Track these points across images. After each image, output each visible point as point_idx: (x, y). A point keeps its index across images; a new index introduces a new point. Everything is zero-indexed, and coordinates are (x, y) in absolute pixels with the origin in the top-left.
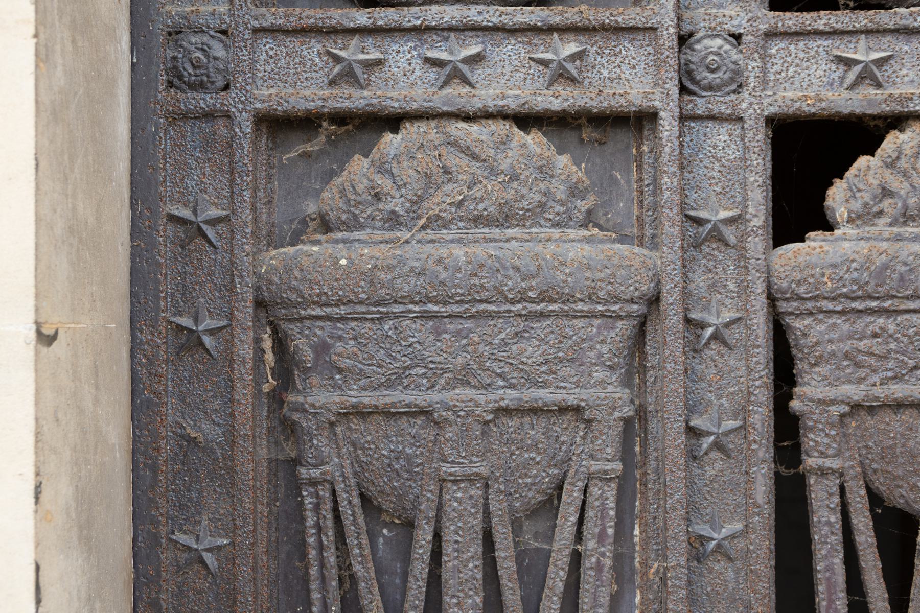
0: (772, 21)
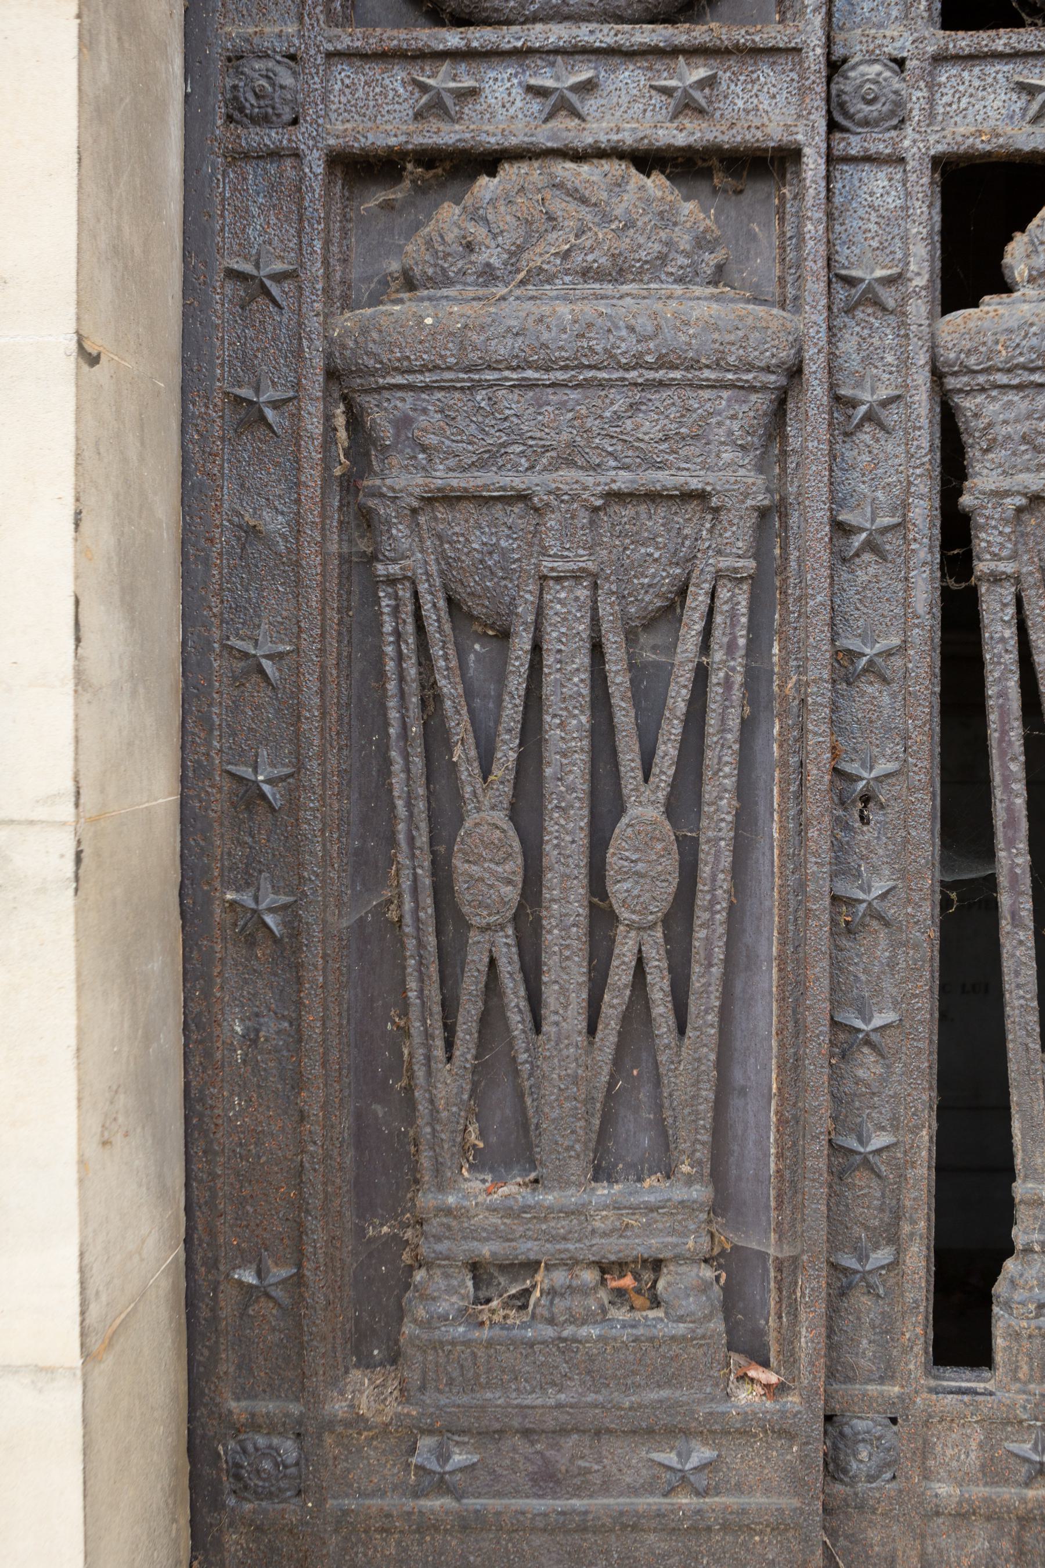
0: (942, 42)
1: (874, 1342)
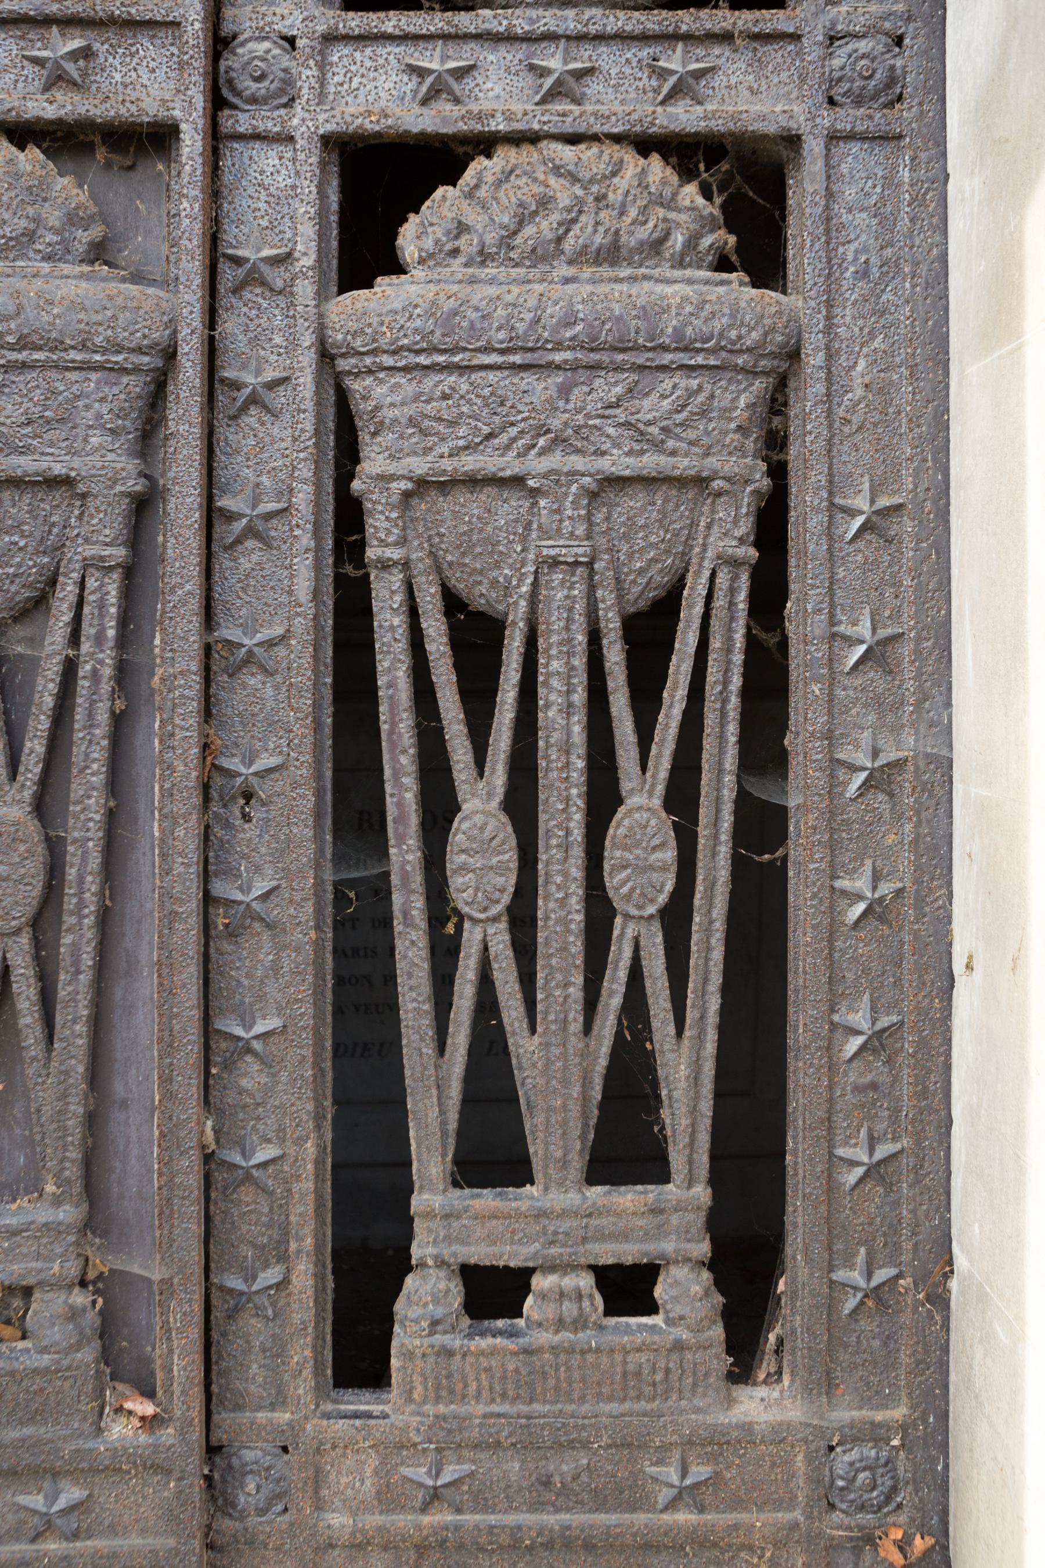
0: (332, 21)
1: (264, 1366)
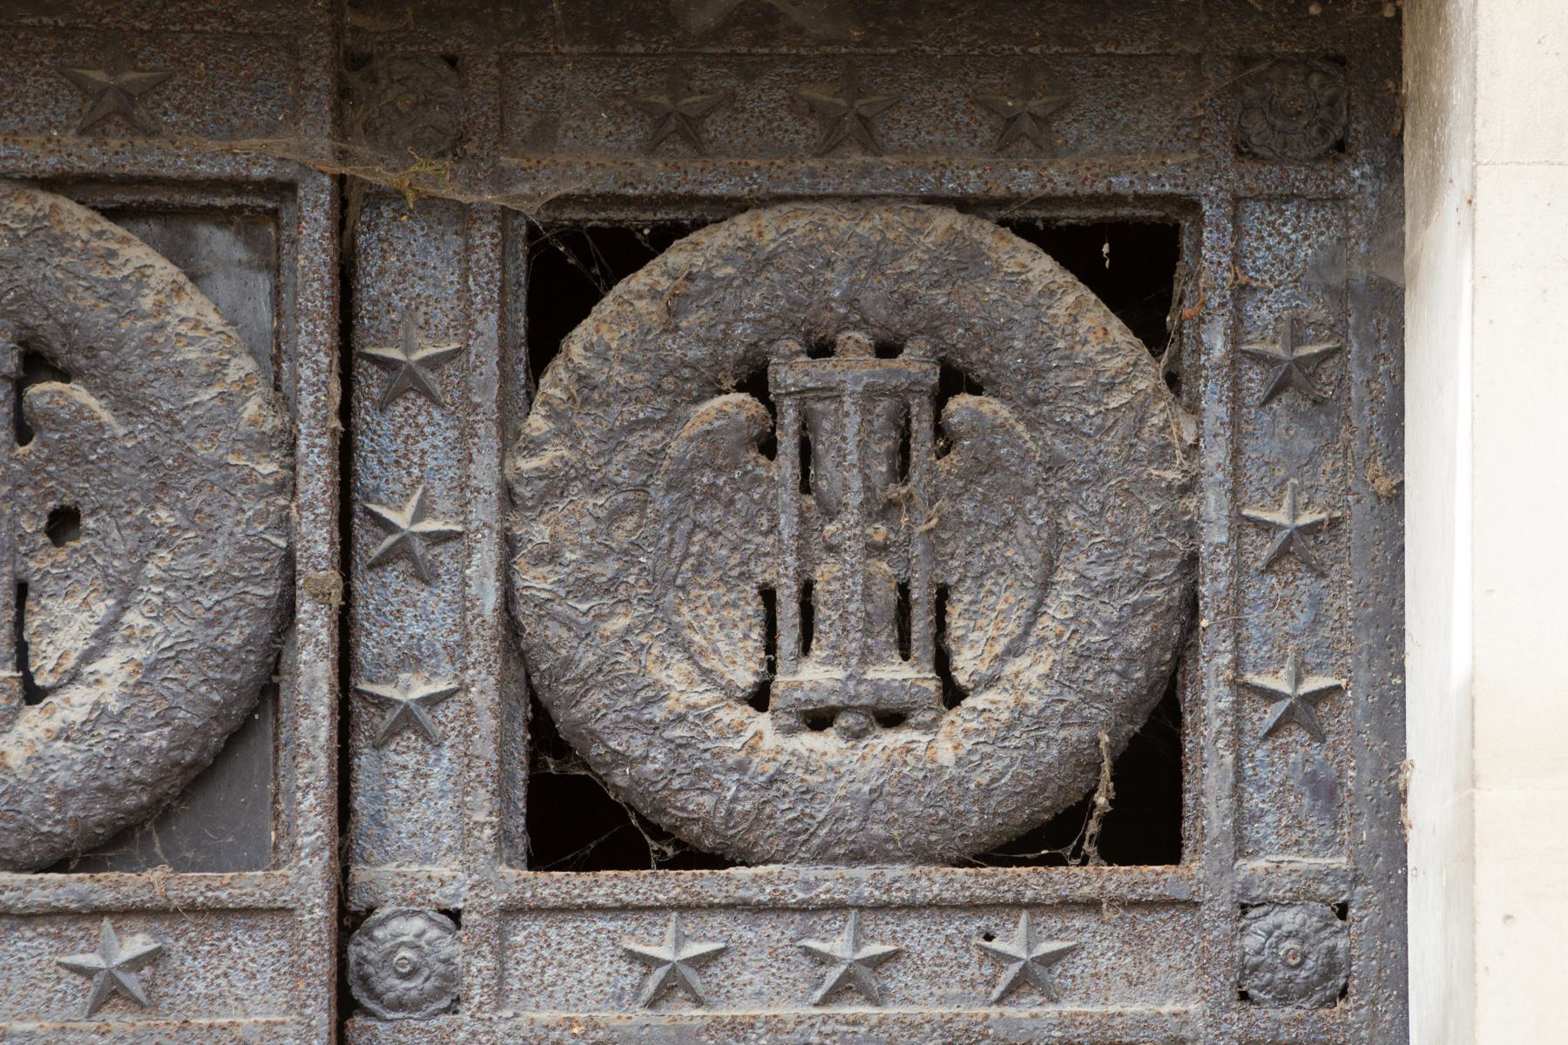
0: (514, 889)
